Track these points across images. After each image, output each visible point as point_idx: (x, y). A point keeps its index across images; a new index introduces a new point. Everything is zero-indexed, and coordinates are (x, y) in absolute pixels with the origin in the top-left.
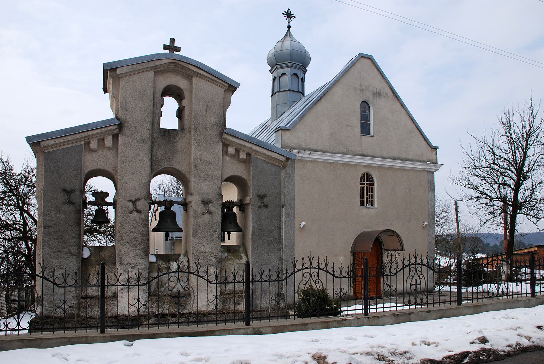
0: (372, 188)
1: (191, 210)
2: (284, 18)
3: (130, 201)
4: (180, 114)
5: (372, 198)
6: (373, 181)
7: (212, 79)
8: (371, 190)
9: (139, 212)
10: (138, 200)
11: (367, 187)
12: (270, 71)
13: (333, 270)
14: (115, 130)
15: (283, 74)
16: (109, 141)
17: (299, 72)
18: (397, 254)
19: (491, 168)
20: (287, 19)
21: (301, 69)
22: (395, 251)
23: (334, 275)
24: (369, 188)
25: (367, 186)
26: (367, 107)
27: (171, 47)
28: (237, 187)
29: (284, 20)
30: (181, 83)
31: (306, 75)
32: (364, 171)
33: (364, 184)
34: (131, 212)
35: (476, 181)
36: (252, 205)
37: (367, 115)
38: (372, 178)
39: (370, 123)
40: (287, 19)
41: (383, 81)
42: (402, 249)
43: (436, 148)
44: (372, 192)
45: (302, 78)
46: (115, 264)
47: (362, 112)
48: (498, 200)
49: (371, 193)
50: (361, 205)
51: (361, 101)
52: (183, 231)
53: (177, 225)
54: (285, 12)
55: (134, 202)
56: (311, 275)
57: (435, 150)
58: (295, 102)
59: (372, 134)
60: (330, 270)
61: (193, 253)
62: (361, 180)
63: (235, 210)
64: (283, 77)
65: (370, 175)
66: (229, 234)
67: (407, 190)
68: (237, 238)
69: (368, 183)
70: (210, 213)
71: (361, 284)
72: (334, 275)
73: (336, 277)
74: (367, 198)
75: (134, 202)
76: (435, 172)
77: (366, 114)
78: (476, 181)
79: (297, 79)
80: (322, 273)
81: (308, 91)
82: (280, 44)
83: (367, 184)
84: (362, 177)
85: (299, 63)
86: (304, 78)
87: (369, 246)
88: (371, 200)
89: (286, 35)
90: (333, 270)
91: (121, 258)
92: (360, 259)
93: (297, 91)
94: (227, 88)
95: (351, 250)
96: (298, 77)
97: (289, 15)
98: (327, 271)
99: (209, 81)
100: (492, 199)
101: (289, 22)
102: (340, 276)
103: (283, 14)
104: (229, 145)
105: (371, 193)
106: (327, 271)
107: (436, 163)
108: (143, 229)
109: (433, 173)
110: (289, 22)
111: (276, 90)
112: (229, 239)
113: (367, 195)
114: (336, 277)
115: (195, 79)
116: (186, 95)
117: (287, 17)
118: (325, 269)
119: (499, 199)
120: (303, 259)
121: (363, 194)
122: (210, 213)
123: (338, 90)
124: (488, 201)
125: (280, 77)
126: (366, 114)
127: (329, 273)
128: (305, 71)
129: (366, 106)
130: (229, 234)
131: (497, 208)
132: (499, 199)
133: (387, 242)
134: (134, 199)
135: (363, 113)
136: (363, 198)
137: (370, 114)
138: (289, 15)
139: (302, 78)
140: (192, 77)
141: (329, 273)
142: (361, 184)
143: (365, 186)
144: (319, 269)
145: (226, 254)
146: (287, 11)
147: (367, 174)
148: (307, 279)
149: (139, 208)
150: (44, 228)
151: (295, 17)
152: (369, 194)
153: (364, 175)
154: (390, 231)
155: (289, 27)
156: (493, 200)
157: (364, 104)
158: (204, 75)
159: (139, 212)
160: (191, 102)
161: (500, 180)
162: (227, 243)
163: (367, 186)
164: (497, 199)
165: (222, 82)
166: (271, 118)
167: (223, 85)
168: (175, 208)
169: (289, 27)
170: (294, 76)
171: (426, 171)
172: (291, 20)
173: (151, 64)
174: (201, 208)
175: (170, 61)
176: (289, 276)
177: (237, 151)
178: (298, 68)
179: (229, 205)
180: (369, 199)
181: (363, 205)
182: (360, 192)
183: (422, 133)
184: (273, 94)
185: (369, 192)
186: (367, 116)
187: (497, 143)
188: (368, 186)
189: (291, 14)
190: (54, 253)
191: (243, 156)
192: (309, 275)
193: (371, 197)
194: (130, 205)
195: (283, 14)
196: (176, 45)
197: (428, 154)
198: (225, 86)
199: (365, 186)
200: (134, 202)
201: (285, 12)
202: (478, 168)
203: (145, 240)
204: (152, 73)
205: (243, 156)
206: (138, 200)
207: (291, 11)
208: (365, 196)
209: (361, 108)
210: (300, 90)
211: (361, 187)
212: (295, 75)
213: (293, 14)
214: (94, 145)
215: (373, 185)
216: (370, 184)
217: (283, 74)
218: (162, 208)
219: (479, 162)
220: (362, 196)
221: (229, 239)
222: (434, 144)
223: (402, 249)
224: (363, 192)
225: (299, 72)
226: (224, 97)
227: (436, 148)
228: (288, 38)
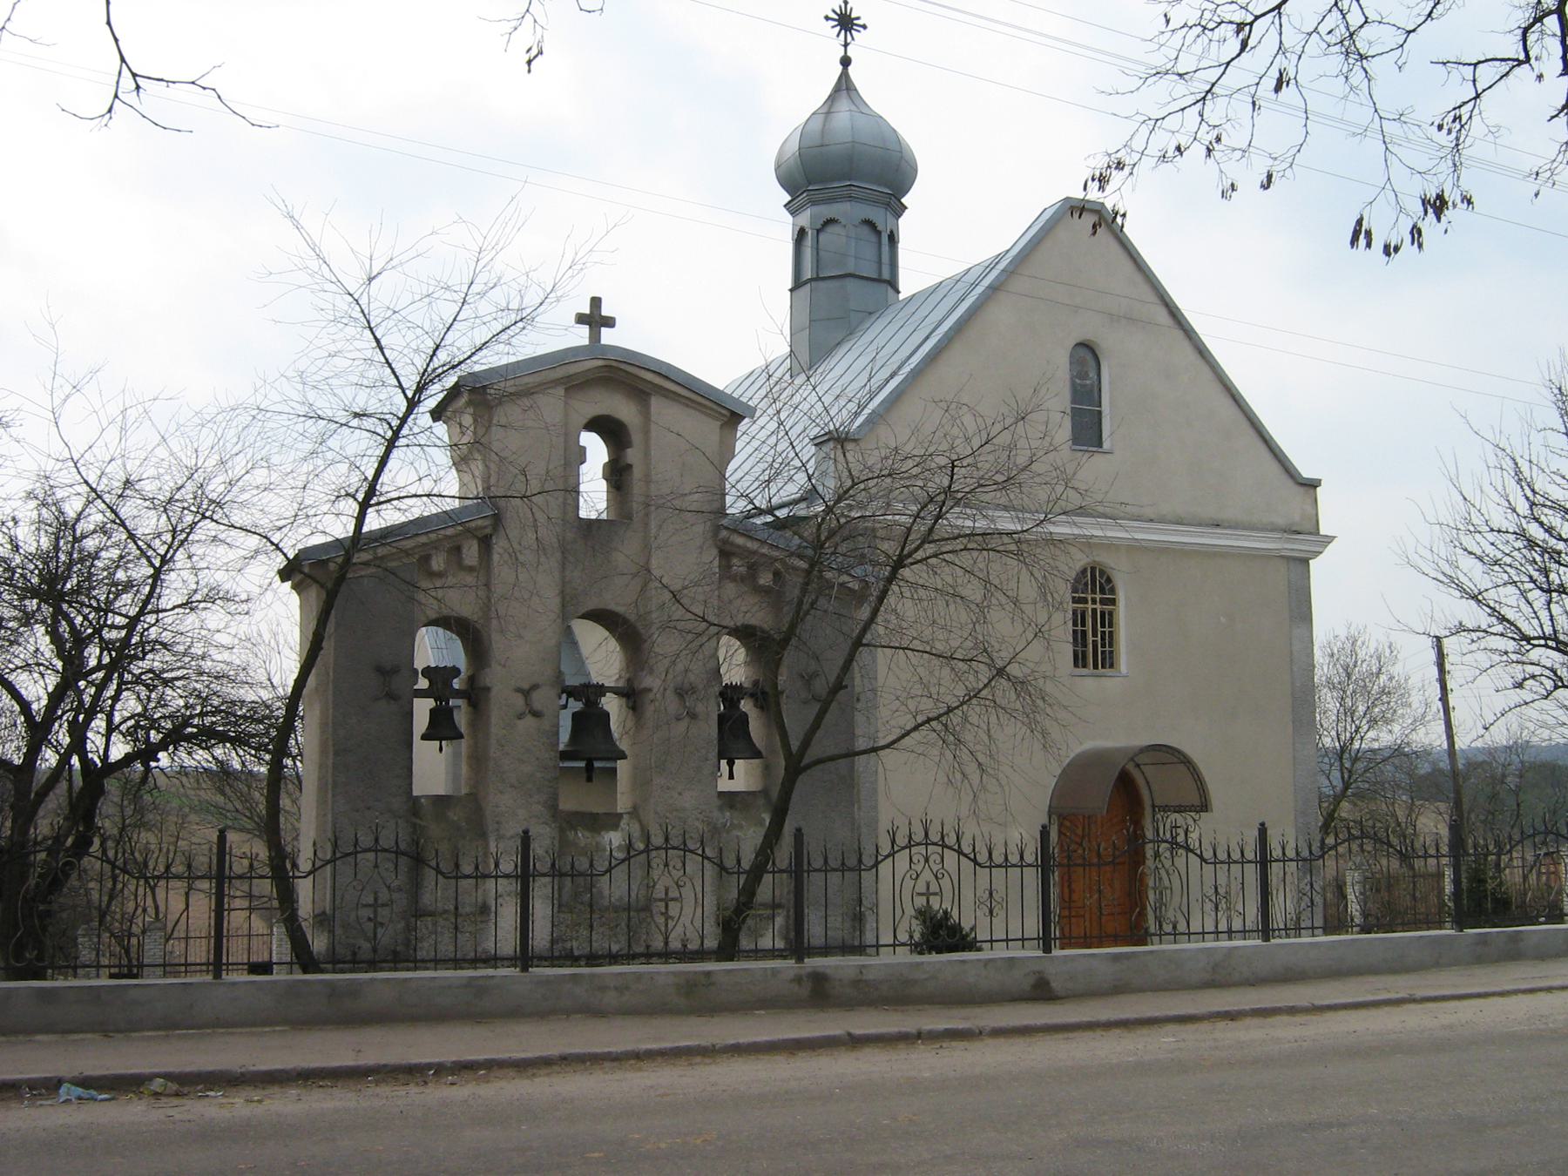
0: (1111, 614)
1: (649, 711)
2: (830, 29)
3: (519, 690)
4: (616, 474)
5: (1111, 645)
6: (1112, 591)
7: (693, 401)
8: (1107, 619)
9: (537, 714)
10: (535, 687)
11: (1094, 611)
12: (785, 206)
13: (974, 850)
14: (485, 527)
15: (830, 222)
16: (471, 552)
17: (878, 215)
18: (1190, 821)
19: (1521, 534)
20: (838, 35)
21: (888, 204)
22: (1185, 811)
23: (975, 861)
24: (1103, 614)
25: (1094, 606)
26: (1092, 363)
27: (595, 319)
28: (748, 650)
29: (830, 42)
30: (623, 409)
31: (903, 222)
32: (1080, 560)
33: (1085, 601)
34: (520, 716)
35: (1476, 575)
36: (787, 697)
37: (1092, 385)
38: (1109, 580)
39: (1100, 413)
40: (838, 35)
41: (1138, 278)
42: (1204, 807)
43: (1313, 485)
44: (1111, 626)
45: (892, 232)
46: (483, 835)
47: (1076, 377)
48: (1546, 646)
49: (1107, 629)
50: (1076, 665)
51: (1078, 341)
52: (461, 736)
53: (454, 723)
54: (834, 11)
55: (526, 693)
56: (927, 860)
57: (1312, 491)
58: (870, 313)
59: (1106, 445)
60: (967, 849)
61: (656, 813)
62: (1075, 590)
63: (746, 705)
64: (831, 229)
65: (1102, 573)
66: (731, 764)
67: (1223, 619)
68: (746, 773)
69: (1098, 596)
70: (693, 716)
71: (1084, 916)
72: (975, 861)
73: (980, 865)
74: (1095, 643)
75: (528, 692)
76: (1311, 561)
77: (1088, 382)
78: (1476, 575)
79: (873, 238)
80: (951, 857)
81: (910, 281)
82: (817, 125)
83: (1094, 601)
84: (1077, 580)
85: (879, 185)
86: (895, 232)
87: (1098, 799)
88: (1107, 649)
89: (837, 89)
90: (974, 850)
91: (498, 823)
92: (1076, 835)
93: (875, 276)
94: (725, 419)
95: (1050, 806)
96: (879, 233)
97: (846, 22)
98: (960, 852)
99: (687, 406)
100: (1528, 639)
101: (846, 45)
102: (988, 864)
103: (827, 18)
104: (733, 554)
105: (1107, 629)
106: (960, 852)
107: (1317, 532)
108: (547, 756)
109: (1305, 562)
110: (846, 45)
111: (808, 274)
112: (731, 777)
113: (1095, 635)
114: (980, 865)
115: (656, 403)
116: (636, 437)
117: (838, 28)
118: (956, 847)
119: (1550, 643)
120: (910, 824)
121: (1084, 633)
122: (693, 716)
123: (1002, 314)
124: (1511, 645)
125: (818, 231)
126: (1088, 382)
127: (966, 856)
128: (900, 210)
129: (1089, 357)
130: (731, 764)
131: (1537, 670)
132: (1550, 643)
133: (1157, 784)
134: (526, 686)
135: (1078, 381)
136: (1085, 645)
137: (1100, 382)
138: (846, 22)
139: (892, 232)
140: (649, 395)
141: (966, 856)
142: (1075, 600)
143: (1090, 606)
144: (944, 846)
145: (728, 814)
146: (840, 7)
147: (1093, 569)
148: (919, 868)
149: (537, 706)
150: (336, 754)
151: (864, 27)
152: (1103, 633)
153: (1084, 571)
154: (1164, 749)
155: (846, 62)
156: (1529, 643)
157: (1083, 352)
158: (674, 393)
159: (537, 714)
160: (647, 454)
161: (1553, 576)
162: (724, 785)
163: (1094, 606)
164: (1542, 642)
165: (715, 407)
166: (791, 368)
167: (720, 413)
168: (611, 704)
169: (846, 62)
170: (866, 230)
171: (1282, 557)
172: (853, 39)
173: (560, 373)
174: (672, 705)
175: (600, 363)
176: (883, 860)
177: (753, 569)
178: (875, 202)
179: (730, 695)
180: (1103, 646)
181: (1084, 666)
182: (1075, 624)
183: (1268, 438)
184: (798, 284)
185: (1103, 626)
186: (1092, 391)
187: (1538, 451)
188: (1098, 606)
189: (853, 16)
190: (357, 811)
191: (765, 579)
192: (922, 860)
193: (1109, 639)
194: (519, 701)
195: (827, 18)
196: (605, 312)
197: (1290, 506)
198: (724, 415)
199: (1090, 606)
200: (526, 693)
201: (834, 11)
202: (1518, 515)
203: (550, 782)
204: (560, 391)
205: (765, 579)
206: (535, 687)
207: (851, 9)
208: (1090, 638)
209: (1071, 363)
210: (886, 275)
211: (1075, 612)
212: (870, 224)
213: (858, 18)
214: (438, 563)
215: (1113, 602)
216: (1103, 602)
217: (830, 222)
218: (576, 706)
219: (1479, 511)
220: (1079, 638)
221: (731, 777)
222: (1306, 472)
223: (1204, 807)
224: (1083, 625)
225: (878, 215)
226: (721, 442)
227: (1313, 485)
228: (843, 105)
